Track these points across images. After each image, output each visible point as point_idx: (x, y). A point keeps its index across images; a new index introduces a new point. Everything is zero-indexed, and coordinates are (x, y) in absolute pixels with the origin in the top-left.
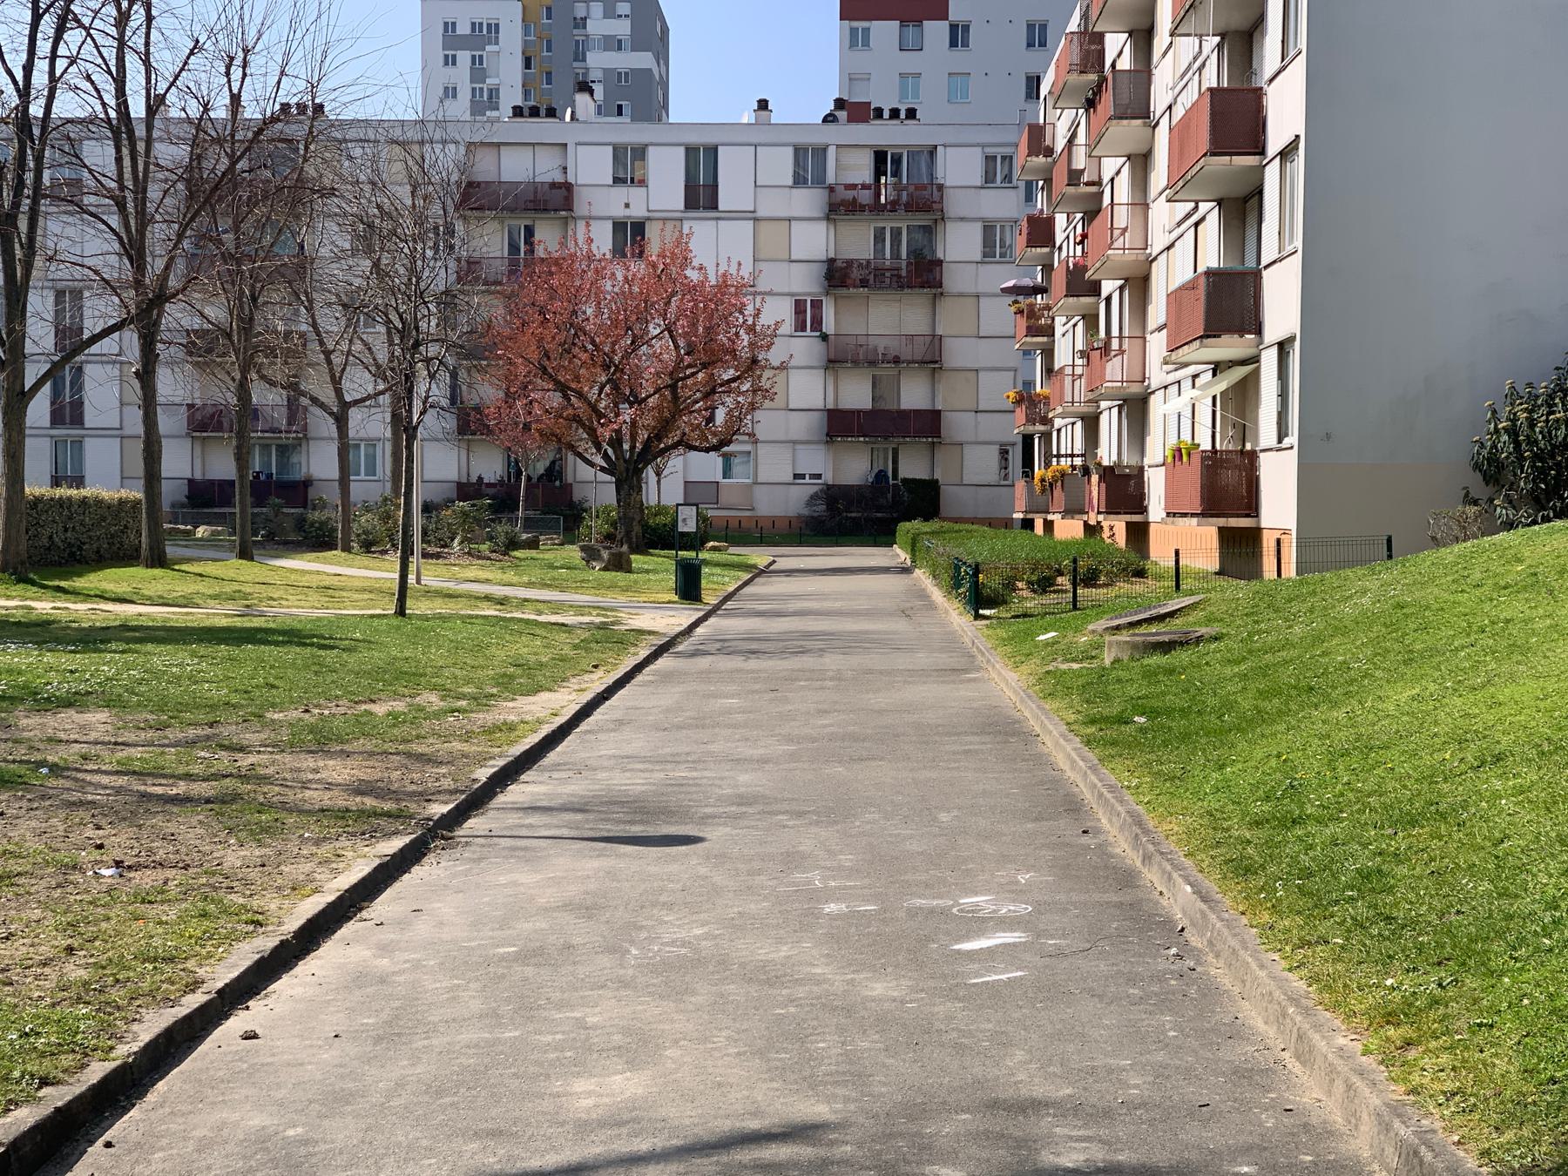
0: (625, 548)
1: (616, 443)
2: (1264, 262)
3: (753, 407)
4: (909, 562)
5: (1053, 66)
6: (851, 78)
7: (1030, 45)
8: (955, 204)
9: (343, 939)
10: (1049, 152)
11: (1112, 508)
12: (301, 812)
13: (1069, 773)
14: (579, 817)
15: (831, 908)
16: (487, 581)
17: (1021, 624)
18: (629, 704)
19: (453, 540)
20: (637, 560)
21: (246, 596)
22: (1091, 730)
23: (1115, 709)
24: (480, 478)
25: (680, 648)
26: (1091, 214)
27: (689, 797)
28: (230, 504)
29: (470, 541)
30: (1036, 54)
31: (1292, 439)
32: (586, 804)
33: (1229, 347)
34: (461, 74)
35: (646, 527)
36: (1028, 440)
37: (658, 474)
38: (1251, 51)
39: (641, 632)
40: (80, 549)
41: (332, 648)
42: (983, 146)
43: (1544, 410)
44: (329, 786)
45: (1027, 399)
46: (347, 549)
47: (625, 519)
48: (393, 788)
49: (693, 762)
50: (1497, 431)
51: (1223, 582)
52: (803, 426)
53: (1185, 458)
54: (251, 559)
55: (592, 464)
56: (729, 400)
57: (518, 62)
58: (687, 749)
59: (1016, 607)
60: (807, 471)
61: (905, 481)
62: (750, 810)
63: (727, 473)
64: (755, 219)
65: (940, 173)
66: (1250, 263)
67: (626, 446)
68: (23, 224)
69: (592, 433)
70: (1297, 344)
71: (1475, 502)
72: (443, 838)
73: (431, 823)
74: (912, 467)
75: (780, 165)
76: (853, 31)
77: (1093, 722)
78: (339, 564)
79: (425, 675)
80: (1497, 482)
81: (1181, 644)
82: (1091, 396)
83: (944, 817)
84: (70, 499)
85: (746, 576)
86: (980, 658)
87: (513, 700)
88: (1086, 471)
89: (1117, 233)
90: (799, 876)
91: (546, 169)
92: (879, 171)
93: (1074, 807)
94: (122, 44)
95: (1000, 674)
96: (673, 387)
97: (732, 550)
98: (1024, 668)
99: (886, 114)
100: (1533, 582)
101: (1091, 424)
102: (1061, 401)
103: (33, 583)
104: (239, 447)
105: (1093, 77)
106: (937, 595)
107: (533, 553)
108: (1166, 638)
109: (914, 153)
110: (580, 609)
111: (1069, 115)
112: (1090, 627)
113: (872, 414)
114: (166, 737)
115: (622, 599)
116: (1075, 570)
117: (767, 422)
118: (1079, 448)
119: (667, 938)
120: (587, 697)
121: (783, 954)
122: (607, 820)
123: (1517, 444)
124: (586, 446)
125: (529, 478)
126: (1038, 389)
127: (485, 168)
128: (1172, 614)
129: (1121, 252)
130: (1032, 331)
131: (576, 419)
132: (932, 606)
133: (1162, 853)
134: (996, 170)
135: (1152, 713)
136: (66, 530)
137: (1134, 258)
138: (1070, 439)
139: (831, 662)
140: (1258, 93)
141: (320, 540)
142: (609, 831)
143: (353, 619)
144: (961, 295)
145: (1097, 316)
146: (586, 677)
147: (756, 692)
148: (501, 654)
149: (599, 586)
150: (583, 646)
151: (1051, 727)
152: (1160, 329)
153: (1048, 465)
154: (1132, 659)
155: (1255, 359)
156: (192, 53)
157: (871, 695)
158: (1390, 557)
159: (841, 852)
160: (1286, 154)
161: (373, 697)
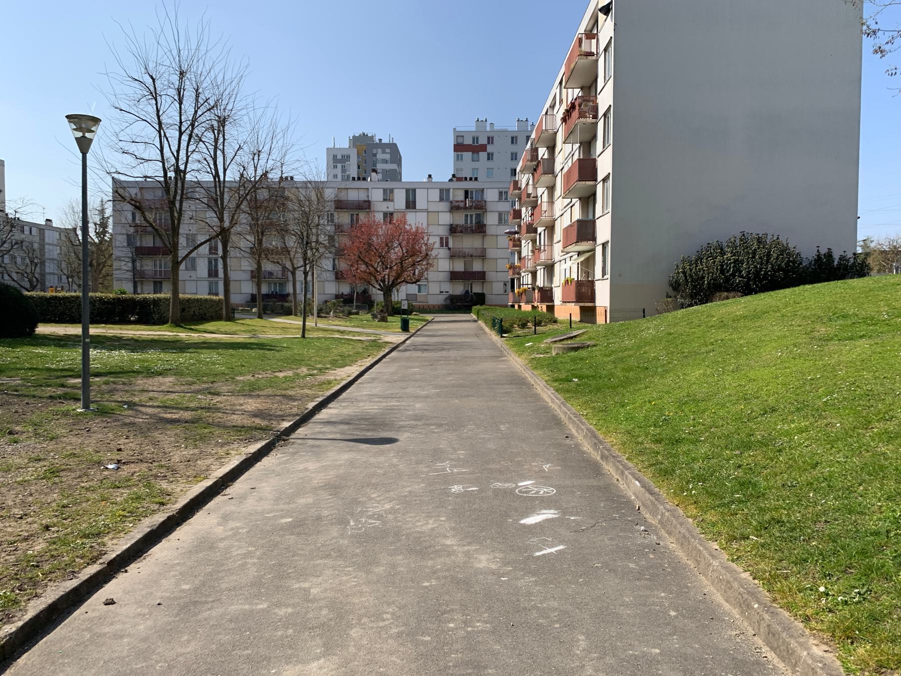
0: (386, 314)
1: (383, 281)
2: (596, 217)
3: (427, 269)
4: (476, 319)
5: (521, 160)
6: (457, 169)
7: (512, 159)
8: (490, 207)
9: (208, 509)
10: (520, 189)
11: (542, 301)
12: (226, 427)
13: (550, 404)
14: (346, 427)
15: (456, 488)
16: (340, 325)
17: (518, 340)
18: (379, 371)
19: (330, 312)
20: (390, 318)
21: (255, 331)
22: (556, 384)
23: (563, 375)
24: (342, 293)
25: (400, 348)
26: (534, 207)
27: (395, 416)
28: (256, 302)
29: (336, 312)
30: (514, 162)
31: (608, 276)
32: (351, 420)
33: (584, 246)
34: (338, 171)
35: (393, 308)
36: (513, 280)
37: (398, 291)
38: (590, 147)
39: (387, 343)
40: (205, 315)
41: (273, 350)
42: (498, 188)
43: (694, 265)
44: (244, 412)
45: (512, 267)
46: (296, 315)
47: (386, 305)
48: (271, 413)
49: (399, 398)
50: (678, 272)
51: (583, 325)
52: (443, 276)
53: (569, 283)
54: (262, 318)
55: (375, 287)
56: (419, 267)
57: (356, 167)
58: (397, 391)
59: (515, 333)
60: (444, 290)
61: (474, 293)
62: (420, 423)
63: (419, 292)
64: (428, 212)
65: (485, 197)
66: (591, 217)
67: (386, 283)
68: (177, 205)
69: (375, 277)
70: (610, 244)
71: (670, 297)
72: (284, 440)
73: (279, 433)
74: (477, 289)
75: (435, 195)
76: (458, 156)
77: (556, 381)
78: (293, 320)
79: (304, 360)
80: (677, 290)
81: (582, 348)
82: (535, 265)
83: (502, 427)
84: (201, 299)
85: (424, 323)
86: (504, 352)
87: (335, 370)
88: (534, 289)
89: (543, 212)
90: (439, 465)
91: (362, 196)
92: (466, 197)
93: (557, 422)
94: (216, 148)
95: (513, 359)
96: (401, 263)
97: (421, 315)
98: (522, 356)
99: (468, 179)
100: (722, 325)
101: (534, 274)
102: (525, 267)
103: (182, 327)
104: (258, 282)
105: (535, 163)
106: (487, 329)
107: (357, 316)
108: (576, 346)
109: (477, 191)
110: (368, 335)
111: (527, 176)
112: (545, 341)
113: (464, 272)
114: (191, 389)
115: (383, 331)
116: (535, 321)
117: (431, 275)
118: (530, 282)
119: (371, 511)
120: (363, 368)
121: (430, 526)
122: (358, 429)
123: (686, 277)
124: (373, 282)
125: (357, 293)
126: (516, 264)
127: (343, 196)
128: (575, 336)
129: (545, 218)
130: (514, 246)
131: (370, 273)
132: (485, 333)
133: (614, 457)
134: (502, 195)
135: (580, 377)
136: (200, 309)
137: (549, 219)
138: (527, 279)
139: (453, 354)
140: (594, 161)
141: (288, 312)
142: (357, 435)
143: (286, 339)
144: (492, 235)
145: (536, 240)
146: (365, 360)
147: (426, 366)
148: (336, 351)
149: (377, 327)
150: (366, 348)
151: (539, 383)
152: (558, 242)
153: (519, 288)
154: (563, 353)
155: (594, 250)
156: (238, 150)
157: (467, 367)
158: (644, 317)
159: (459, 449)
160: (605, 180)
161: (281, 370)
